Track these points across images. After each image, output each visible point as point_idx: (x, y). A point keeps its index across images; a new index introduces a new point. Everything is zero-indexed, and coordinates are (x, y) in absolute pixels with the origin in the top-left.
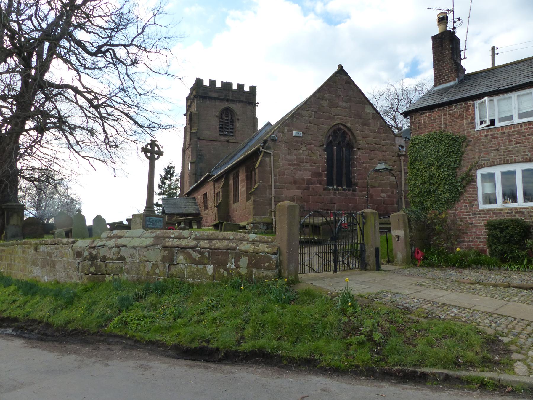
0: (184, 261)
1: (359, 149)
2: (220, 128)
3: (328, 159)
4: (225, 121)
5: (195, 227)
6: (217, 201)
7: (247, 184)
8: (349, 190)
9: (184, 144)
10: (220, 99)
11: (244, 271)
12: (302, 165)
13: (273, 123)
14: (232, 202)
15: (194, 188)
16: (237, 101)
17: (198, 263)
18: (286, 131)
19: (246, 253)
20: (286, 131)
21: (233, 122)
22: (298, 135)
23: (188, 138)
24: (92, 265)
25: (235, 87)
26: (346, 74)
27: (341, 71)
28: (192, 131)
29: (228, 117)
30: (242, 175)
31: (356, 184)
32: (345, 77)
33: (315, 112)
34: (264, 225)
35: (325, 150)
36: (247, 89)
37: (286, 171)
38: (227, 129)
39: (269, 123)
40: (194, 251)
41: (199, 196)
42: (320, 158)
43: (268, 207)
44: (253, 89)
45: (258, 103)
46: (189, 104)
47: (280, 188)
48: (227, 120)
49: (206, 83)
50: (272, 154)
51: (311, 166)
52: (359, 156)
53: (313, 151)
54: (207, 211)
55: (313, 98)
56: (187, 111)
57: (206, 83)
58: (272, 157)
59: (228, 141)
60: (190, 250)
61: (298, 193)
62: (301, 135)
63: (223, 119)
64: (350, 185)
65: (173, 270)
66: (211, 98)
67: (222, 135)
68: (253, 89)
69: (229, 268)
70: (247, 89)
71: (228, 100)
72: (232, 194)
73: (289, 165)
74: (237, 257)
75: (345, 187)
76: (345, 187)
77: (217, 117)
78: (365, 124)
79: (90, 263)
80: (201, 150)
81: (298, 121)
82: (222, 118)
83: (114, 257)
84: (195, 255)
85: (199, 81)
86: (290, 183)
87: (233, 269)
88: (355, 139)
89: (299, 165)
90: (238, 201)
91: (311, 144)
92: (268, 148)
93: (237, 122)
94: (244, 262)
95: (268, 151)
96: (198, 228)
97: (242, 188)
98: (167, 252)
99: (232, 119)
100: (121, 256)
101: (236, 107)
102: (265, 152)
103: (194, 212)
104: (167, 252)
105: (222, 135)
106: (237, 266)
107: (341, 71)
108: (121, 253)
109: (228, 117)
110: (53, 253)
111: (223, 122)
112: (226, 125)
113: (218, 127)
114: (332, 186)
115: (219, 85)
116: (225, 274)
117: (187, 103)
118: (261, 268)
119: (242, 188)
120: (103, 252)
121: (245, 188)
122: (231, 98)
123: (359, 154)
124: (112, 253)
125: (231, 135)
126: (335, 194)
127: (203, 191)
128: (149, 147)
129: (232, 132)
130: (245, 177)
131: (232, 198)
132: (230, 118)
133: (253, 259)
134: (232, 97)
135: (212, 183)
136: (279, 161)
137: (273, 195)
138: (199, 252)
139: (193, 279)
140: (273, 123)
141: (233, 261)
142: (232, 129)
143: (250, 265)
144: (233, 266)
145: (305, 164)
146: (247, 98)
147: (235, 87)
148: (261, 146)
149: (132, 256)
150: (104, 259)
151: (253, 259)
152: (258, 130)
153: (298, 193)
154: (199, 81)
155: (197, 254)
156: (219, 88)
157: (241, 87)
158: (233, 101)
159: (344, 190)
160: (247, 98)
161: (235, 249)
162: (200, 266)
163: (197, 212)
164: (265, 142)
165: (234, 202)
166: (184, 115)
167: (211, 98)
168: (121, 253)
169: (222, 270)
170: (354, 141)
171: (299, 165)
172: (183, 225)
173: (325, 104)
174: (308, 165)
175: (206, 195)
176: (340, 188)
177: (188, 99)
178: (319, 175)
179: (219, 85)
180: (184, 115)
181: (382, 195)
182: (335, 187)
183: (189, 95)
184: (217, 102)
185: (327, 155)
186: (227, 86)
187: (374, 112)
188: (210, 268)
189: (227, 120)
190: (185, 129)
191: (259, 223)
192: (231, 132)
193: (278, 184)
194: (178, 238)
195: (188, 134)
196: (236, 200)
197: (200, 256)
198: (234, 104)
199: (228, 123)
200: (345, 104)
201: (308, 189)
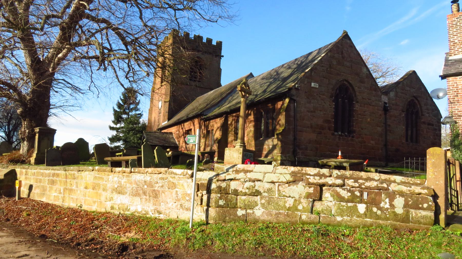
0: (331, 199)
1: (357, 102)
3: (335, 108)
8: (350, 136)
11: (399, 210)
17: (348, 201)
18: (306, 82)
19: (402, 194)
20: (306, 82)
22: (315, 86)
24: (220, 198)
25: (205, 40)
26: (350, 39)
27: (346, 37)
31: (354, 132)
32: (348, 41)
35: (333, 101)
36: (214, 43)
40: (343, 189)
42: (329, 107)
44: (220, 44)
52: (357, 108)
60: (338, 189)
62: (317, 87)
64: (351, 132)
65: (318, 206)
68: (220, 44)
69: (383, 207)
70: (214, 43)
71: (198, 51)
73: (308, 111)
74: (392, 196)
75: (346, 134)
76: (346, 134)
78: (362, 82)
79: (219, 195)
83: (247, 191)
84: (345, 194)
87: (387, 209)
88: (355, 94)
89: (315, 112)
91: (324, 95)
94: (399, 202)
98: (312, 189)
100: (256, 190)
101: (205, 58)
104: (312, 189)
106: (392, 206)
107: (346, 37)
108: (256, 188)
110: (157, 183)
114: (337, 132)
116: (379, 212)
118: (420, 209)
120: (234, 185)
123: (357, 107)
124: (245, 186)
126: (339, 139)
133: (410, 199)
138: (349, 191)
139: (342, 216)
141: (387, 200)
143: (406, 206)
144: (387, 206)
147: (205, 40)
149: (269, 191)
150: (236, 193)
151: (410, 199)
155: (346, 192)
157: (209, 41)
159: (346, 136)
161: (387, 189)
162: (350, 204)
168: (256, 188)
169: (375, 209)
170: (354, 95)
171: (315, 112)
173: (335, 63)
174: (322, 113)
176: (343, 134)
178: (328, 121)
181: (372, 142)
182: (340, 133)
185: (335, 105)
186: (199, 38)
187: (368, 73)
188: (362, 208)
194: (402, 183)
197: (349, 194)
200: (348, 64)
201: (320, 133)
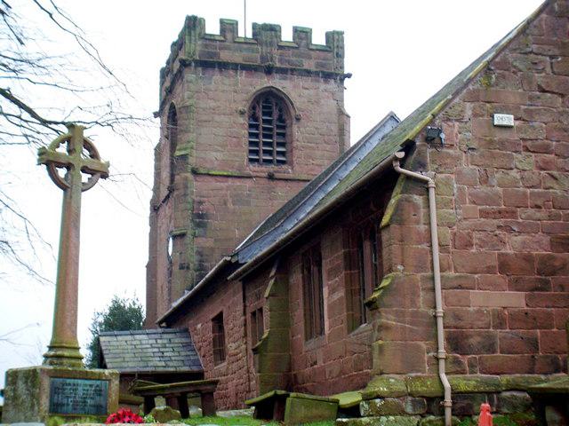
2: (251, 143)
4: (262, 125)
5: (194, 411)
6: (254, 336)
7: (349, 281)
9: (156, 189)
10: (249, 68)
12: (523, 215)
13: (402, 116)
14: (300, 336)
15: (185, 302)
16: (292, 70)
20: (469, 113)
21: (284, 128)
23: (166, 174)
25: (287, 36)
28: (178, 153)
29: (270, 114)
30: (333, 257)
33: (552, 57)
34: (414, 403)
36: (318, 39)
37: (475, 235)
38: (270, 144)
39: (392, 117)
41: (201, 326)
43: (423, 345)
44: (335, 39)
45: (349, 76)
46: (167, 84)
47: (460, 287)
48: (270, 119)
49: (213, 28)
50: (432, 183)
51: (550, 217)
53: (555, 173)
54: (223, 366)
55: (544, 16)
56: (163, 104)
57: (213, 28)
58: (432, 192)
59: (271, 177)
61: (515, 300)
63: (256, 119)
66: (223, 66)
67: (257, 160)
68: (335, 39)
70: (318, 39)
71: (269, 71)
72: (299, 313)
73: (485, 214)
77: (242, 113)
80: (200, 203)
81: (503, 83)
82: (254, 117)
85: (193, 24)
86: (490, 270)
90: (322, 332)
92: (421, 166)
93: (295, 128)
95: (417, 174)
96: (204, 414)
97: (332, 291)
99: (281, 119)
102: (409, 178)
103: (186, 369)
105: (257, 160)
109: (270, 114)
111: (256, 127)
112: (265, 136)
113: (246, 140)
115: (245, 32)
117: (162, 84)
119: (332, 291)
121: (341, 294)
122: (278, 65)
125: (279, 161)
127: (211, 311)
128: (63, 149)
129: (283, 154)
130: (341, 262)
131: (302, 324)
132: (275, 116)
134: (280, 61)
135: (239, 285)
136: (437, 216)
137: (440, 309)
140: (402, 116)
142: (283, 145)
145: (530, 211)
146: (326, 62)
147: (287, 36)
148: (396, 159)
152: (352, 144)
153: (515, 300)
154: (193, 24)
156: (246, 42)
157: (302, 34)
158: (283, 71)
160: (326, 62)
163: (195, 369)
164: (408, 147)
165: (309, 336)
166: (156, 115)
167: (223, 66)
171: (513, 214)
172: (160, 405)
175: (218, 320)
177: (164, 73)
179: (245, 32)
180: (156, 115)
183: (168, 63)
184: (242, 77)
186: (266, 33)
189: (269, 122)
190: (158, 152)
191: (400, 395)
192: (279, 153)
193: (452, 274)
195: (166, 161)
196: (314, 327)
198: (285, 79)
199: (270, 130)
201: (544, 286)
